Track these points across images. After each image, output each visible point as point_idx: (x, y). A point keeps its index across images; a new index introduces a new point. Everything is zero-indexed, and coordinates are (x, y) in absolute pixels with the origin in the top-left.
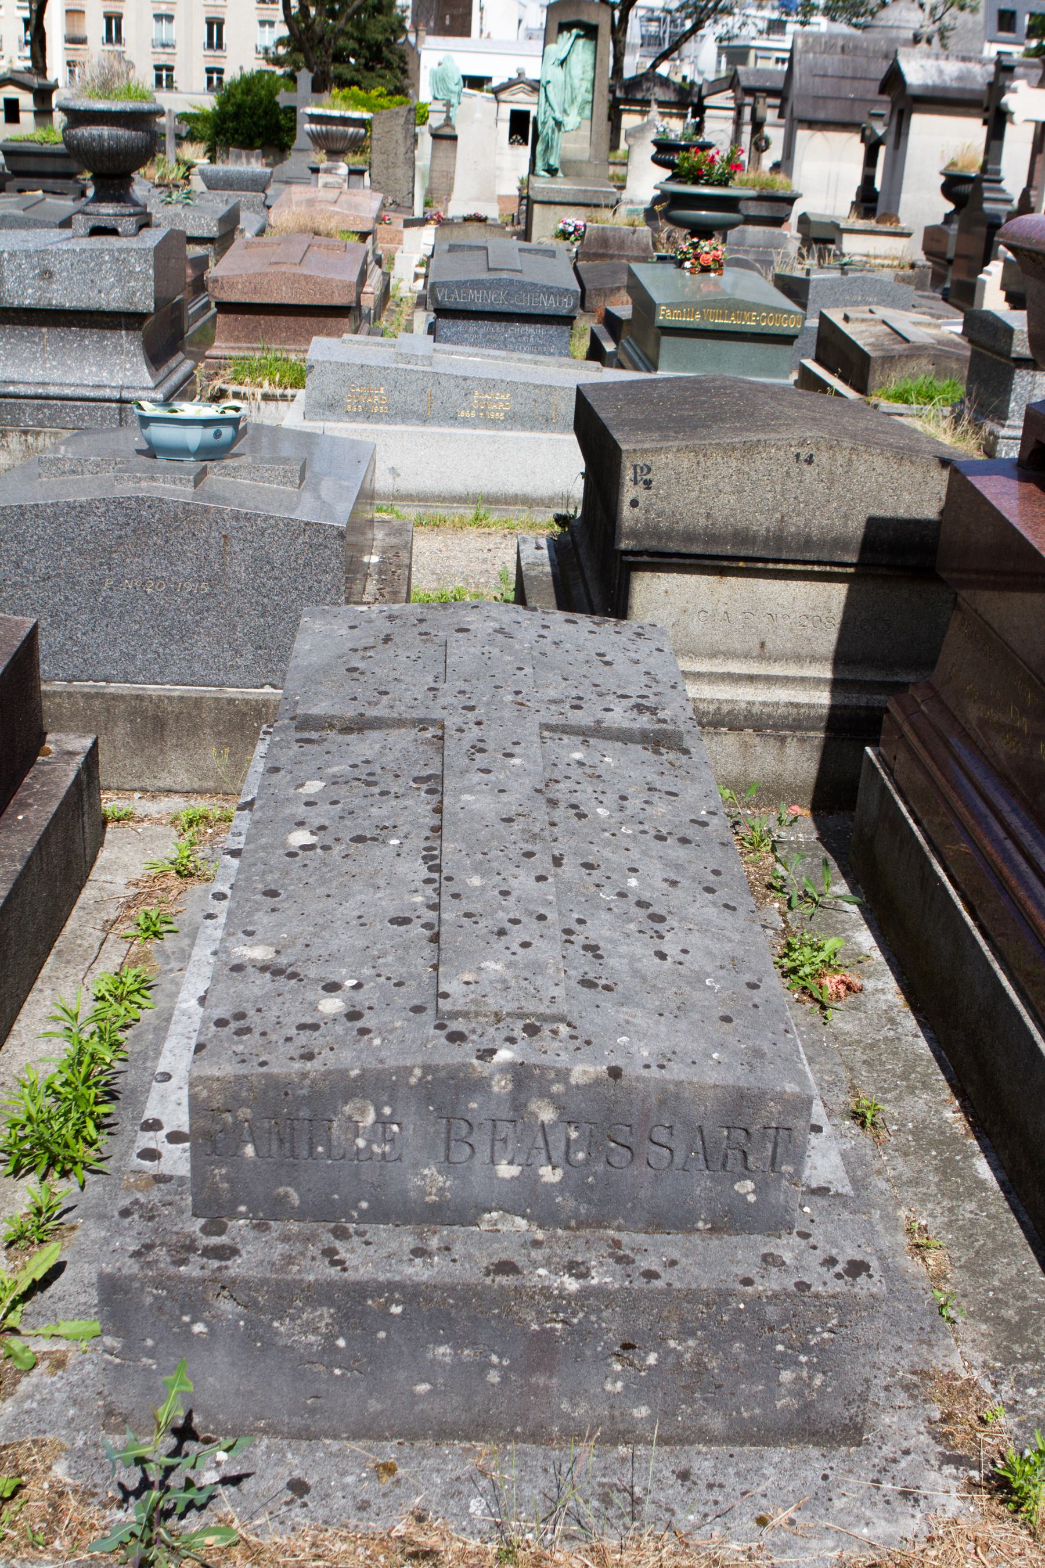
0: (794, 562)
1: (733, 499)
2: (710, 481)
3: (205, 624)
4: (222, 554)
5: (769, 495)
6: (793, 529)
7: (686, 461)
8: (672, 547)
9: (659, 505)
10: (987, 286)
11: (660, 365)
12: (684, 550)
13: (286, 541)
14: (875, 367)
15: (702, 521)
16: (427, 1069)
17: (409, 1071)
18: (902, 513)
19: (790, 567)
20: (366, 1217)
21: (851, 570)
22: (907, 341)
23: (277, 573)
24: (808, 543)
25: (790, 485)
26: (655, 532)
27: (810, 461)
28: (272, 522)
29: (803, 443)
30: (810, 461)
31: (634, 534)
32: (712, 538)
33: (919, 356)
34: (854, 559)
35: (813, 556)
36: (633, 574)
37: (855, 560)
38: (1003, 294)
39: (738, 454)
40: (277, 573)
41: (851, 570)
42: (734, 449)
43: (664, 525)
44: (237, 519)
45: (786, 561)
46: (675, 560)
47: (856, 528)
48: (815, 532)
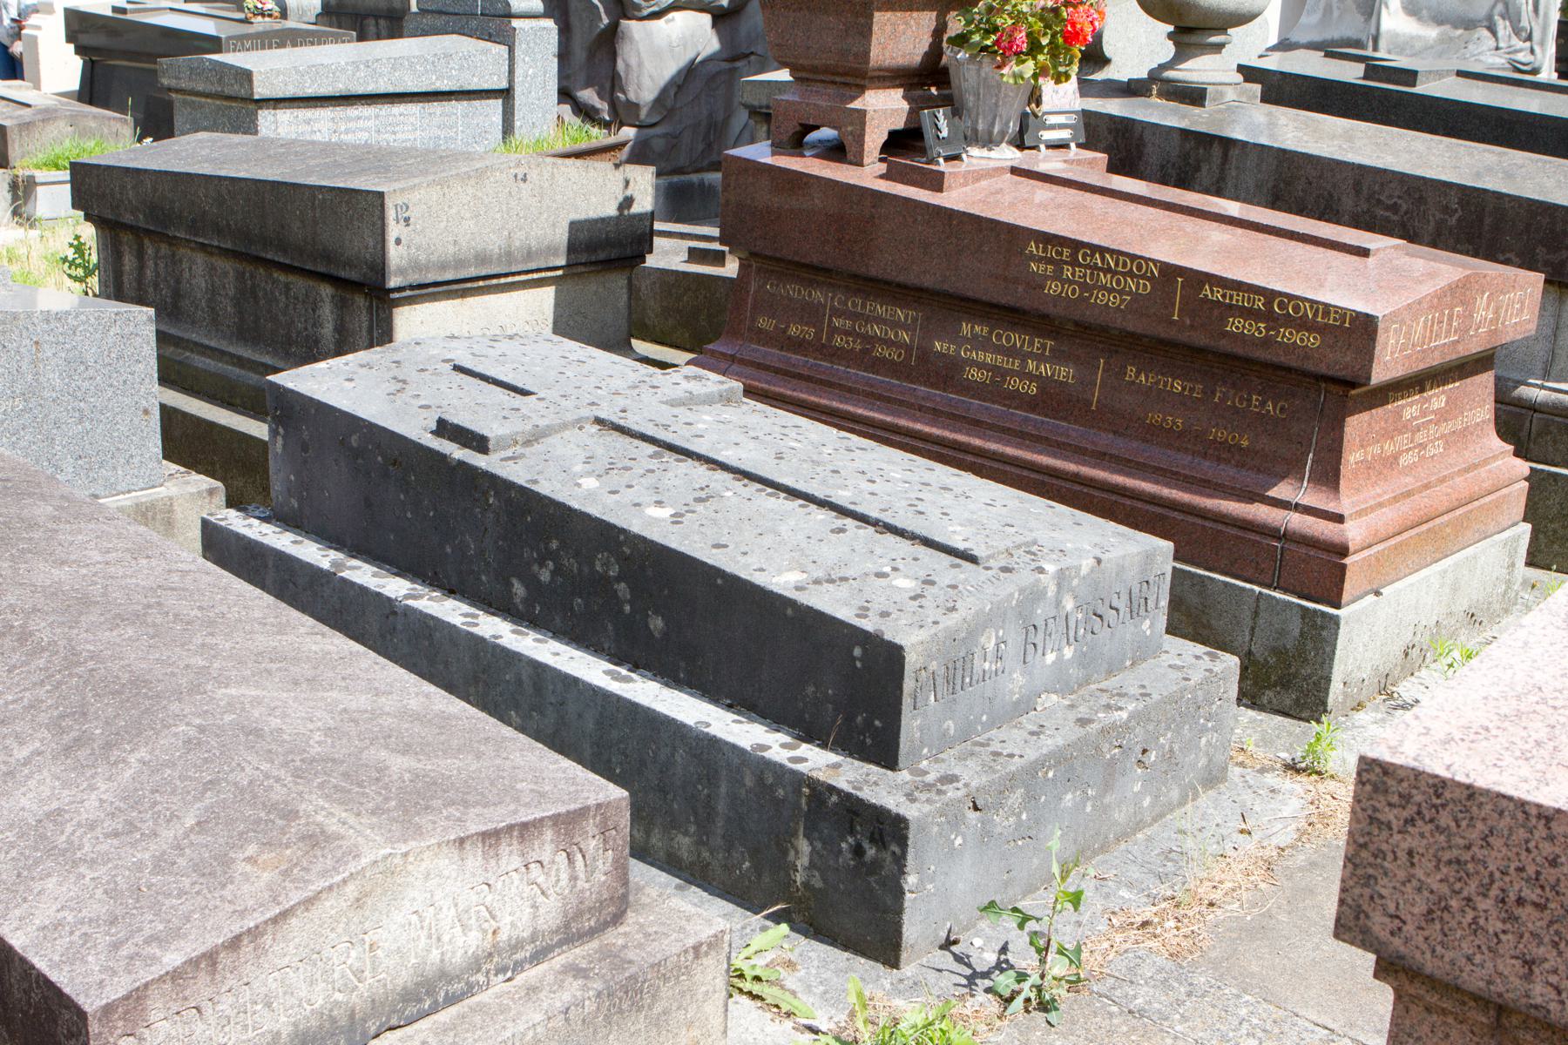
0: (519, 273)
1: (471, 223)
2: (454, 211)
3: (23, 444)
4: (34, 363)
5: (498, 216)
6: (517, 244)
7: (435, 194)
8: (431, 277)
9: (417, 240)
10: (39, 41)
11: (178, 121)
12: (440, 279)
13: (98, 336)
14: (13, 137)
15: (451, 249)
16: (1021, 591)
17: (1011, 595)
18: (592, 215)
19: (517, 278)
20: (989, 726)
21: (560, 273)
22: (29, 106)
23: (91, 372)
24: (530, 255)
25: (513, 203)
26: (416, 266)
27: (524, 180)
28: (83, 317)
29: (519, 164)
30: (524, 180)
31: (401, 271)
32: (460, 263)
33: (55, 119)
34: (562, 262)
35: (533, 266)
36: (395, 311)
37: (563, 262)
38: (72, 46)
39: (473, 181)
40: (91, 372)
41: (560, 273)
42: (469, 177)
43: (423, 258)
44: (48, 321)
45: (513, 274)
46: (431, 290)
47: (561, 236)
48: (533, 243)
